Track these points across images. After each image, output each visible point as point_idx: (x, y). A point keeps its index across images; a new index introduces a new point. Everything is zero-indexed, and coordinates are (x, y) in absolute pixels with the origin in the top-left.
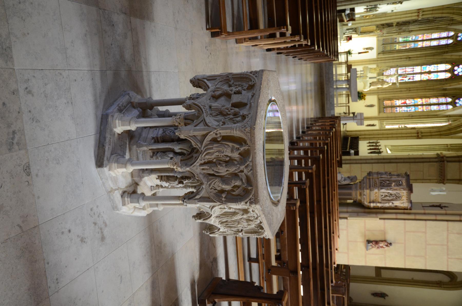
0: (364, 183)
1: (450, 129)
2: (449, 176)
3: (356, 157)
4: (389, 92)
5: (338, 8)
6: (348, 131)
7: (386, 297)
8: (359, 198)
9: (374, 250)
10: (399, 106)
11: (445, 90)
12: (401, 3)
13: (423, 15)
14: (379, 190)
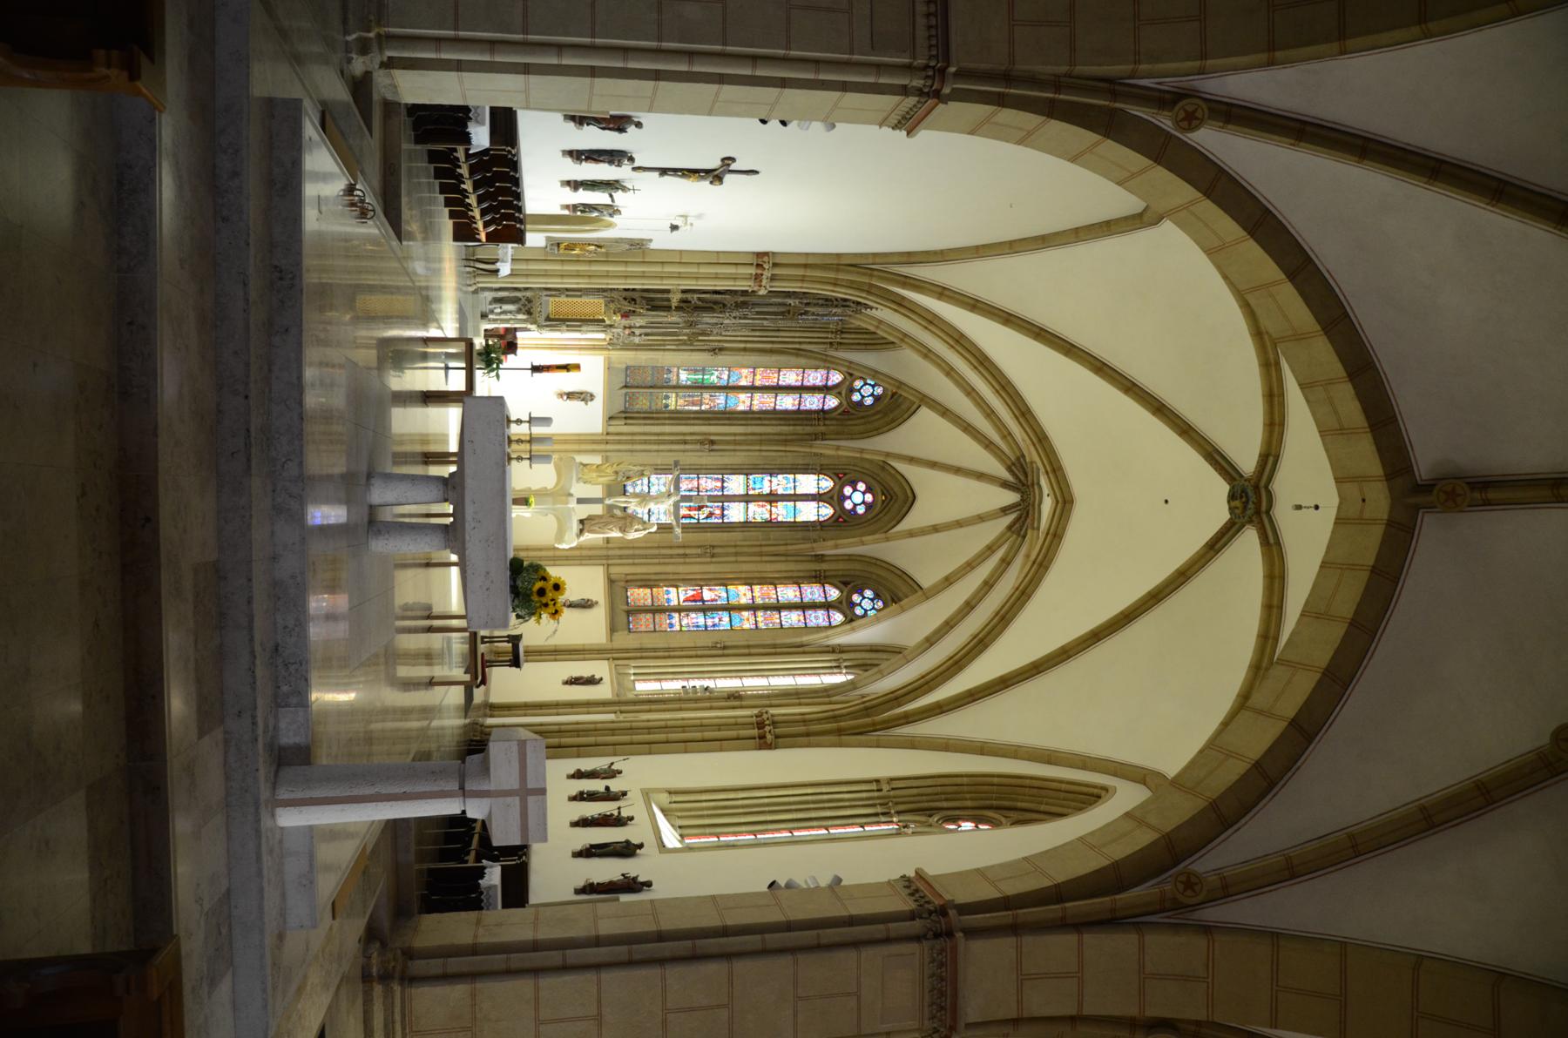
4: (646, 556)
10: (679, 610)
11: (820, 558)
13: (773, 278)
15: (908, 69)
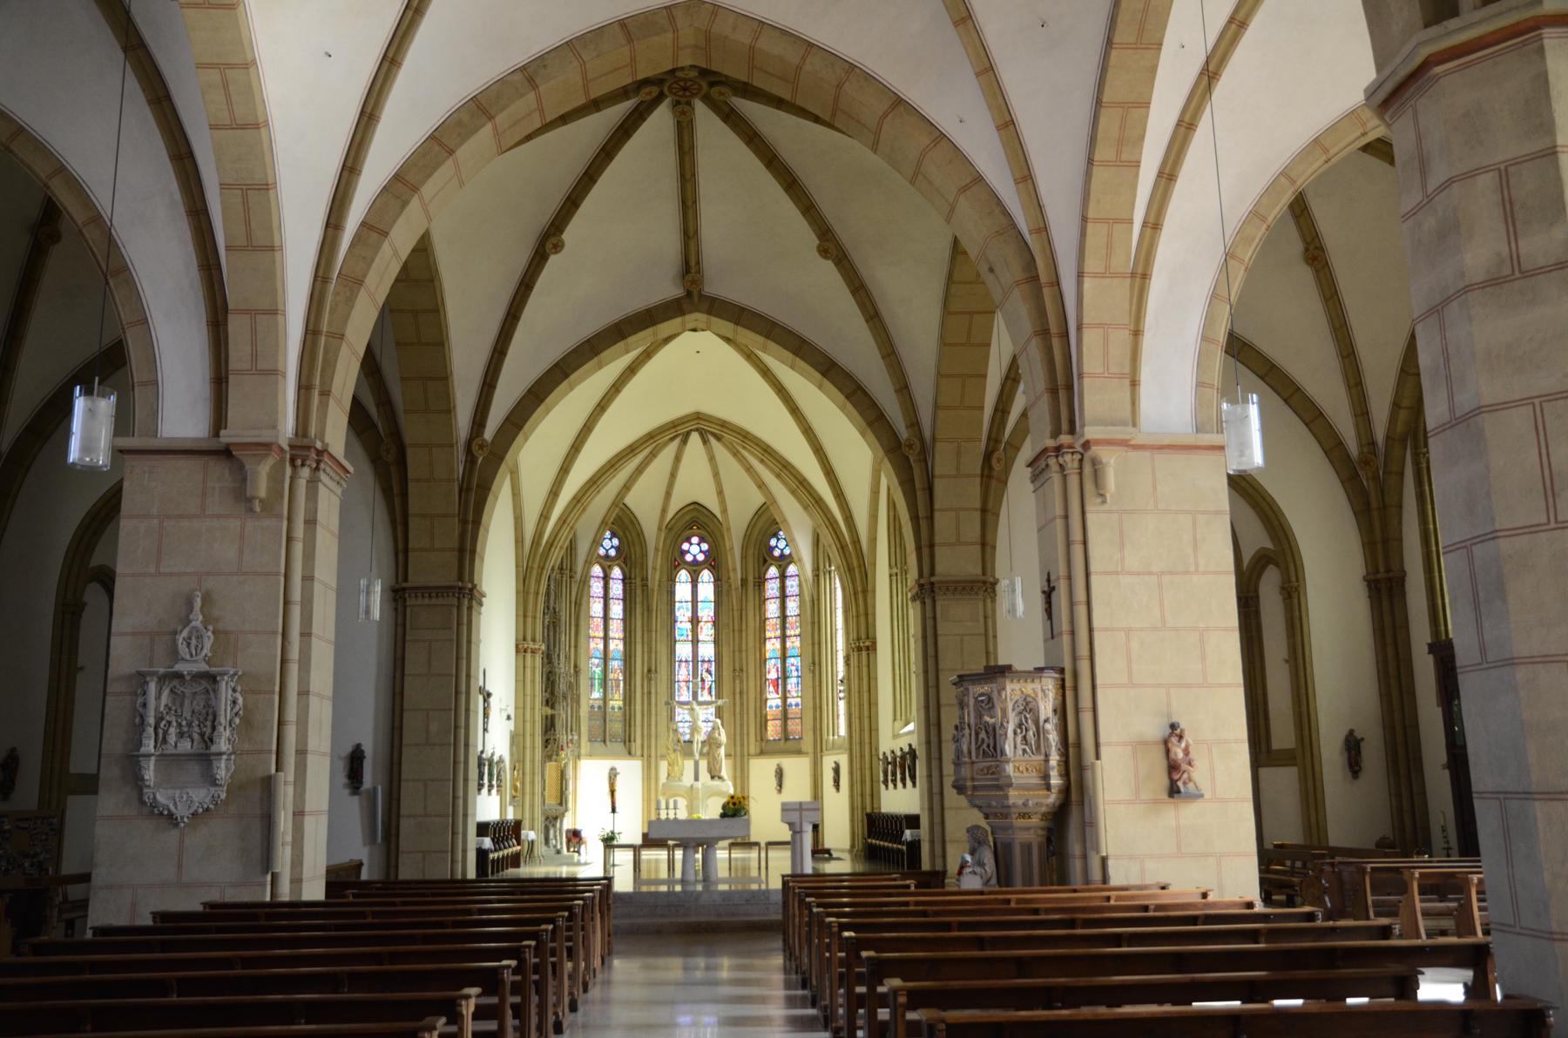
0: (990, 806)
1: (850, 569)
2: (974, 570)
3: (924, 822)
5: (472, 874)
6: (853, 846)
7: (1358, 735)
8: (1035, 820)
9: (1199, 774)
10: (784, 698)
11: (744, 582)
12: (489, 695)
13: (534, 640)
14: (1008, 762)
15: (459, 608)
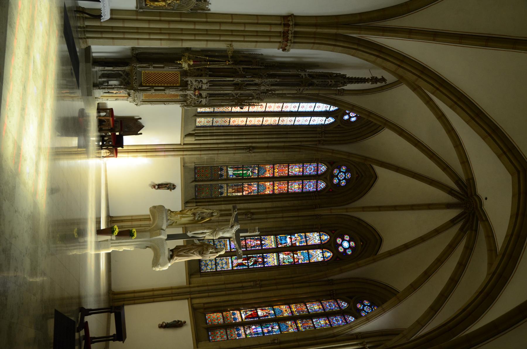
10: (243, 324)
11: (331, 282)
